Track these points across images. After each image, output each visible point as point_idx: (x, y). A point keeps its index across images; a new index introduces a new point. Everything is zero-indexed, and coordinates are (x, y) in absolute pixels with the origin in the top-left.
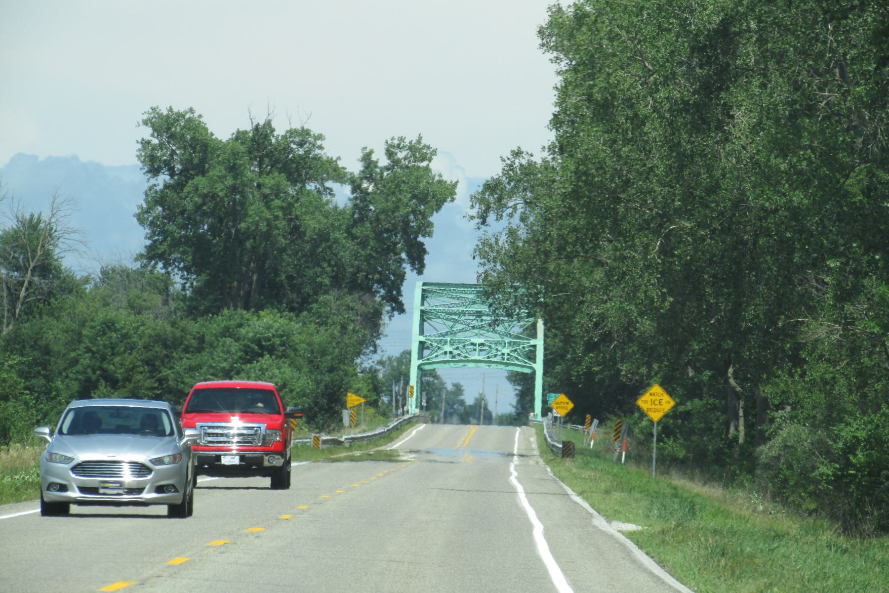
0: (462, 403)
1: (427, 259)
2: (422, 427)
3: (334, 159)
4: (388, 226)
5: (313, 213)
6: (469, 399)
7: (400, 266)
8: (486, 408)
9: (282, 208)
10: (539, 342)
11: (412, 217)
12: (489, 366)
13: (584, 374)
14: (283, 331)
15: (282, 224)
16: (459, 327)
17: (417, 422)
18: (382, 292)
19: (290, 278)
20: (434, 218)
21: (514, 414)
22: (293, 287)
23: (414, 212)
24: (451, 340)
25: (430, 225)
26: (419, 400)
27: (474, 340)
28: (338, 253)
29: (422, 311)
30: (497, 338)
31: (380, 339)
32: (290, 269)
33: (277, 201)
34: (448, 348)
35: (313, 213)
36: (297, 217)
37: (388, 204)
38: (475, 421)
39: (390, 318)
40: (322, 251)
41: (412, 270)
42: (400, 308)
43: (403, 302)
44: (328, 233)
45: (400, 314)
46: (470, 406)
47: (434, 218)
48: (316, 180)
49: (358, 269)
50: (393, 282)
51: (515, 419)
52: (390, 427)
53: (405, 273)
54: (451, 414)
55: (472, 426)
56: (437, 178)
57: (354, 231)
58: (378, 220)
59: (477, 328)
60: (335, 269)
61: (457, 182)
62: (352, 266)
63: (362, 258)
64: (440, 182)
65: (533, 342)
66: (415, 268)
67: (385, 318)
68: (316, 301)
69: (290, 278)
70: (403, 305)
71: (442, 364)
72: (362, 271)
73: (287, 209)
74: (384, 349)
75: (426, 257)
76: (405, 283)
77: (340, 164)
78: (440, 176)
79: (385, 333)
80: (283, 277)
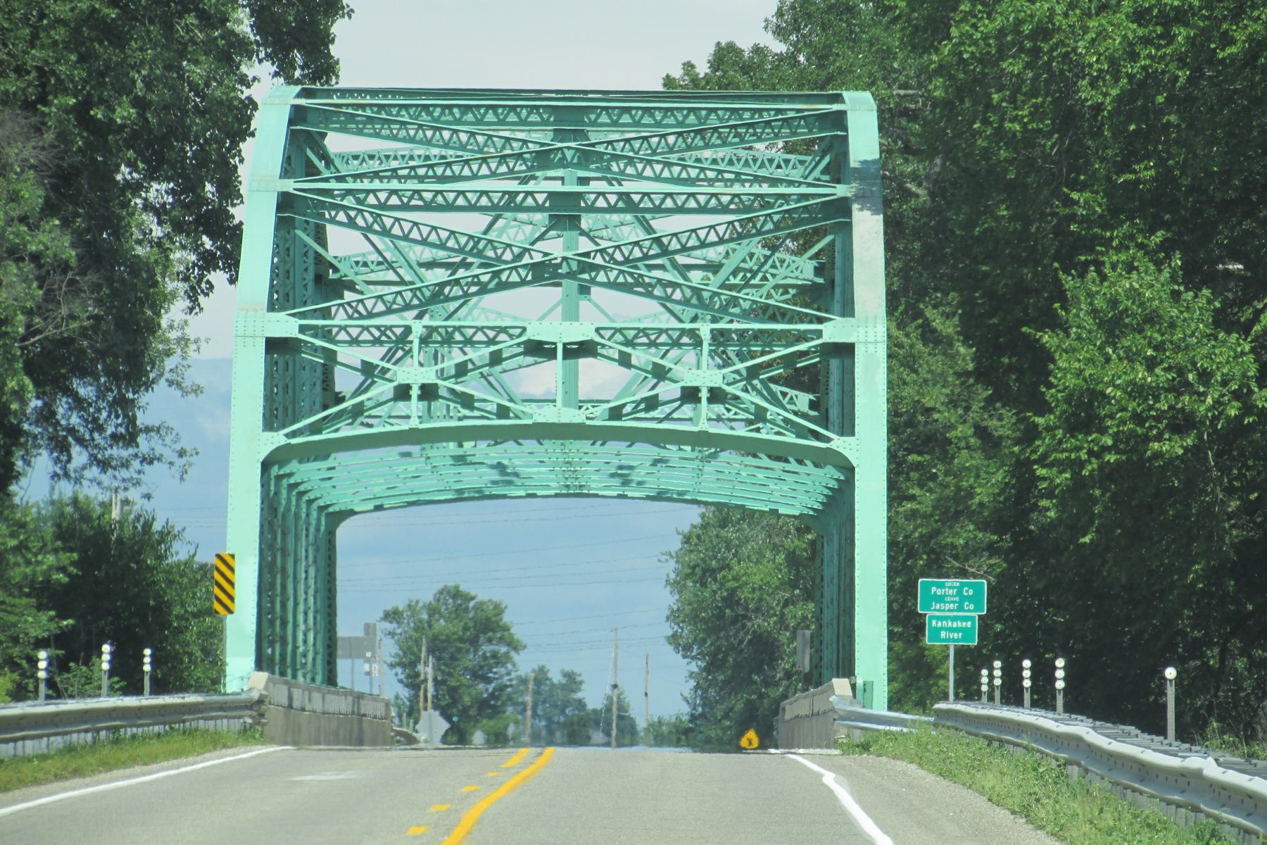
0: (581, 704)
13: (1108, 475)
21: (686, 718)
29: (286, 202)
34: (414, 372)
39: (193, 294)
51: (687, 732)
72: (61, 89)
74: (185, 444)
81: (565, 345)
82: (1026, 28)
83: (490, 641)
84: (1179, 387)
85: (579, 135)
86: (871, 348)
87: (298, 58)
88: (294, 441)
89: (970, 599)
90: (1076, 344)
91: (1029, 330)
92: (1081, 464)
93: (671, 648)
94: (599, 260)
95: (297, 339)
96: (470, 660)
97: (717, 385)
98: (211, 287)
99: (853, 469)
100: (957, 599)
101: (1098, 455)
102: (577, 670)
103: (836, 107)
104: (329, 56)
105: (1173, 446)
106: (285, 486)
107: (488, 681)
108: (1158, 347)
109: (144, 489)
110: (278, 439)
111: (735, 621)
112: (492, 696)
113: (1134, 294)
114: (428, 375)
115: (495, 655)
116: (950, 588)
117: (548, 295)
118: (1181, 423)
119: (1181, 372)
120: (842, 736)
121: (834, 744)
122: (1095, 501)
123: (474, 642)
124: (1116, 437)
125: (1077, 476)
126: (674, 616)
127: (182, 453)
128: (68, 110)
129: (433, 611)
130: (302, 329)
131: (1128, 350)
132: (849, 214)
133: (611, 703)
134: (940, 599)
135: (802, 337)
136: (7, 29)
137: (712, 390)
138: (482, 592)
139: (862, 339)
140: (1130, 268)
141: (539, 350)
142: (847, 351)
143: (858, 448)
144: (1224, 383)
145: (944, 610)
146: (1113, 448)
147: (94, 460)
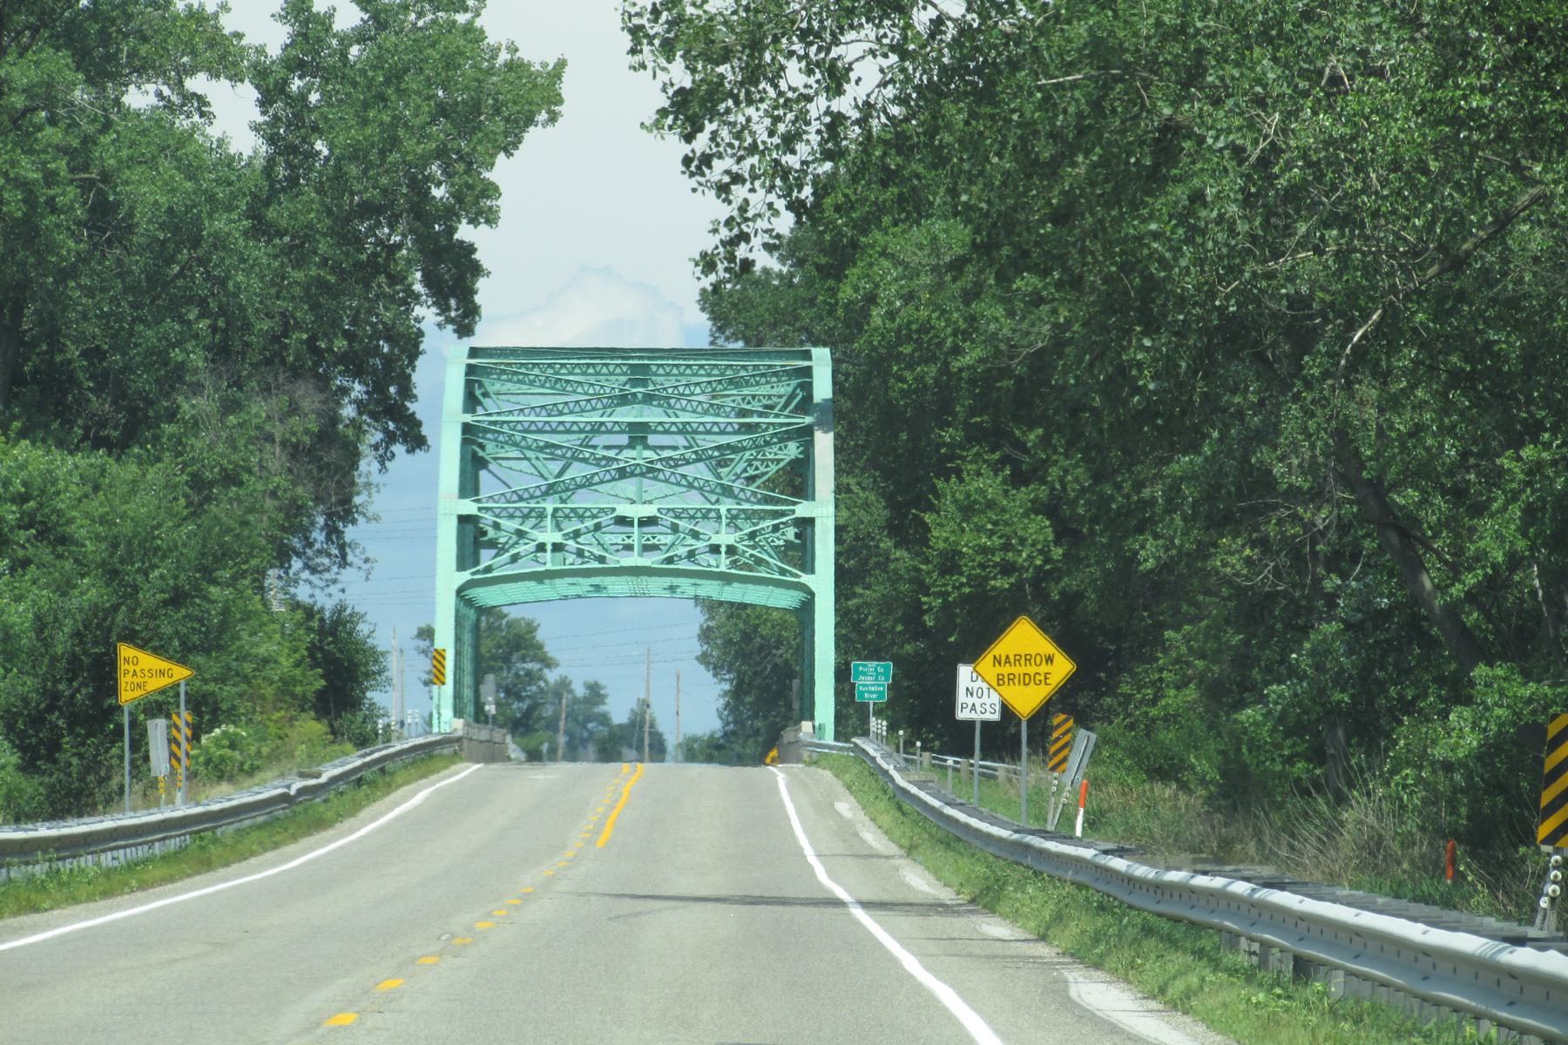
0: (604, 719)
1: (485, 292)
2: (467, 771)
3: (210, 8)
4: (372, 194)
5: (152, 163)
6: (619, 711)
7: (409, 311)
8: (652, 726)
9: (64, 151)
10: (822, 509)
11: (435, 169)
12: (672, 588)
13: (965, 599)
14: (24, 484)
15: (68, 195)
16: (577, 471)
17: (455, 758)
18: (358, 390)
19: (94, 354)
20: (502, 171)
22: (103, 381)
23: (441, 153)
24: (556, 510)
25: (491, 190)
26: (468, 693)
27: (624, 510)
28: (227, 278)
29: (467, 428)
30: (695, 501)
31: (354, 522)
32: (92, 329)
33: (49, 130)
34: (550, 536)
35: (152, 163)
36: (106, 177)
37: (368, 131)
38: (633, 754)
39: (382, 461)
40: (181, 274)
41: (439, 325)
42: (415, 439)
43: (418, 416)
44: (197, 222)
45: (410, 451)
46: (621, 726)
47: (502, 171)
48: (161, 73)
49: (286, 324)
50: (388, 361)
51: (719, 747)
52: (323, 779)
53: (420, 334)
54: (584, 742)
55: (625, 767)
56: (504, 57)
57: (271, 213)
58: (339, 175)
59: (633, 474)
60: (221, 323)
61: (561, 64)
62: (269, 315)
63: (297, 291)
64: (515, 67)
65: (802, 509)
66: (449, 320)
67: (368, 465)
68: (171, 415)
69: (94, 354)
70: (419, 424)
71: (532, 584)
72: (298, 326)
73: (79, 156)
74: (369, 554)
75: (481, 284)
76: (420, 362)
77: (228, 24)
78: (513, 49)
79: (371, 510)
80: (74, 352)
82: (914, 327)
83: (523, 660)
84: (1006, 547)
85: (644, 383)
87: (453, 302)
90: (944, 521)
92: (948, 594)
93: (702, 667)
94: (659, 466)
98: (393, 455)
101: (958, 588)
102: (602, 682)
103: (806, 363)
104: (473, 302)
105: (1002, 583)
108: (995, 523)
109: (340, 586)
110: (466, 576)
113: (981, 491)
114: (557, 538)
115: (529, 673)
117: (628, 487)
118: (1007, 569)
119: (1009, 538)
120: (805, 755)
121: (799, 760)
122: (956, 615)
123: (507, 660)
124: (969, 577)
125: (945, 601)
127: (367, 560)
128: (302, 342)
130: (480, 509)
131: (976, 524)
132: (811, 434)
133: (333, 532)
134: (864, 674)
135: (783, 514)
140: (979, 474)
141: (623, 521)
142: (810, 522)
144: (1033, 545)
146: (967, 584)
147: (307, 566)
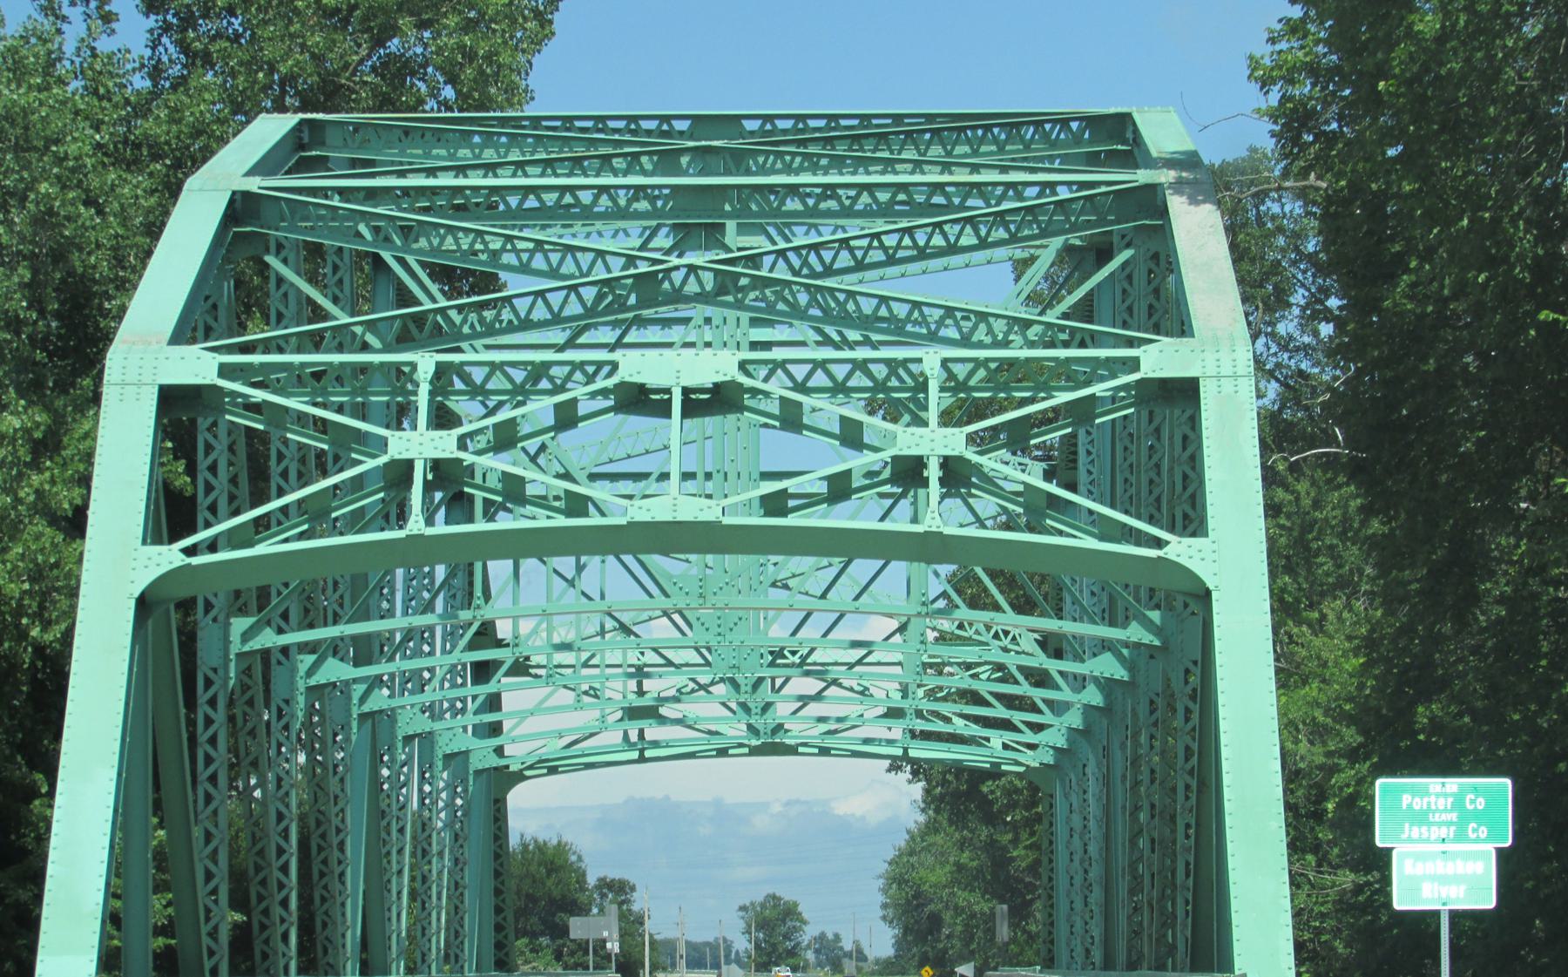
0: (841, 948)
81: (686, 391)
86: (1227, 385)
88: (196, 561)
89: (1477, 816)
91: (1552, 316)
95: (214, 388)
96: (783, 929)
97: (956, 453)
99: (1208, 593)
100: (1454, 816)
106: (302, 690)
107: (790, 940)
110: (170, 556)
111: (918, 906)
112: (793, 948)
116: (1438, 795)
123: (784, 921)
126: (885, 906)
129: (763, 906)
130: (225, 371)
136: (122, 237)
137: (947, 463)
138: (787, 895)
139: (1211, 371)
142: (1184, 392)
143: (1215, 556)
145: (1428, 841)
